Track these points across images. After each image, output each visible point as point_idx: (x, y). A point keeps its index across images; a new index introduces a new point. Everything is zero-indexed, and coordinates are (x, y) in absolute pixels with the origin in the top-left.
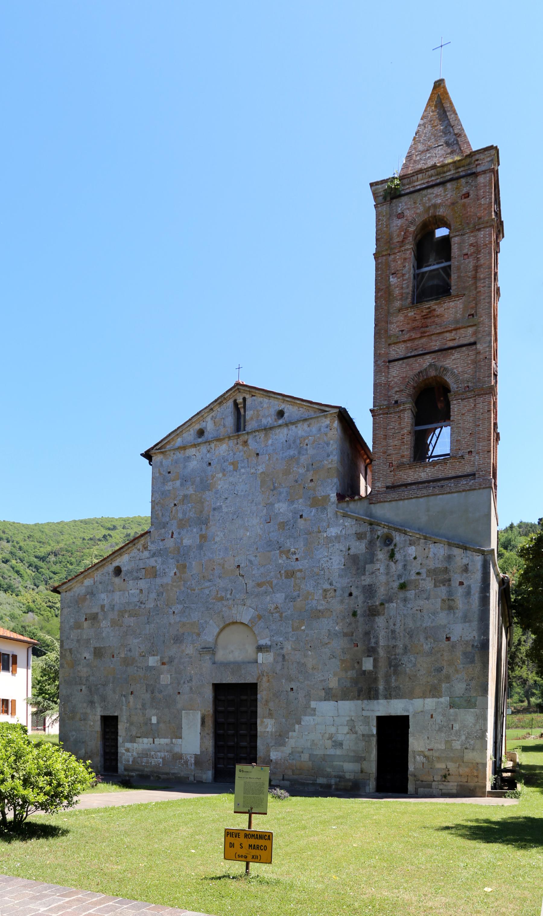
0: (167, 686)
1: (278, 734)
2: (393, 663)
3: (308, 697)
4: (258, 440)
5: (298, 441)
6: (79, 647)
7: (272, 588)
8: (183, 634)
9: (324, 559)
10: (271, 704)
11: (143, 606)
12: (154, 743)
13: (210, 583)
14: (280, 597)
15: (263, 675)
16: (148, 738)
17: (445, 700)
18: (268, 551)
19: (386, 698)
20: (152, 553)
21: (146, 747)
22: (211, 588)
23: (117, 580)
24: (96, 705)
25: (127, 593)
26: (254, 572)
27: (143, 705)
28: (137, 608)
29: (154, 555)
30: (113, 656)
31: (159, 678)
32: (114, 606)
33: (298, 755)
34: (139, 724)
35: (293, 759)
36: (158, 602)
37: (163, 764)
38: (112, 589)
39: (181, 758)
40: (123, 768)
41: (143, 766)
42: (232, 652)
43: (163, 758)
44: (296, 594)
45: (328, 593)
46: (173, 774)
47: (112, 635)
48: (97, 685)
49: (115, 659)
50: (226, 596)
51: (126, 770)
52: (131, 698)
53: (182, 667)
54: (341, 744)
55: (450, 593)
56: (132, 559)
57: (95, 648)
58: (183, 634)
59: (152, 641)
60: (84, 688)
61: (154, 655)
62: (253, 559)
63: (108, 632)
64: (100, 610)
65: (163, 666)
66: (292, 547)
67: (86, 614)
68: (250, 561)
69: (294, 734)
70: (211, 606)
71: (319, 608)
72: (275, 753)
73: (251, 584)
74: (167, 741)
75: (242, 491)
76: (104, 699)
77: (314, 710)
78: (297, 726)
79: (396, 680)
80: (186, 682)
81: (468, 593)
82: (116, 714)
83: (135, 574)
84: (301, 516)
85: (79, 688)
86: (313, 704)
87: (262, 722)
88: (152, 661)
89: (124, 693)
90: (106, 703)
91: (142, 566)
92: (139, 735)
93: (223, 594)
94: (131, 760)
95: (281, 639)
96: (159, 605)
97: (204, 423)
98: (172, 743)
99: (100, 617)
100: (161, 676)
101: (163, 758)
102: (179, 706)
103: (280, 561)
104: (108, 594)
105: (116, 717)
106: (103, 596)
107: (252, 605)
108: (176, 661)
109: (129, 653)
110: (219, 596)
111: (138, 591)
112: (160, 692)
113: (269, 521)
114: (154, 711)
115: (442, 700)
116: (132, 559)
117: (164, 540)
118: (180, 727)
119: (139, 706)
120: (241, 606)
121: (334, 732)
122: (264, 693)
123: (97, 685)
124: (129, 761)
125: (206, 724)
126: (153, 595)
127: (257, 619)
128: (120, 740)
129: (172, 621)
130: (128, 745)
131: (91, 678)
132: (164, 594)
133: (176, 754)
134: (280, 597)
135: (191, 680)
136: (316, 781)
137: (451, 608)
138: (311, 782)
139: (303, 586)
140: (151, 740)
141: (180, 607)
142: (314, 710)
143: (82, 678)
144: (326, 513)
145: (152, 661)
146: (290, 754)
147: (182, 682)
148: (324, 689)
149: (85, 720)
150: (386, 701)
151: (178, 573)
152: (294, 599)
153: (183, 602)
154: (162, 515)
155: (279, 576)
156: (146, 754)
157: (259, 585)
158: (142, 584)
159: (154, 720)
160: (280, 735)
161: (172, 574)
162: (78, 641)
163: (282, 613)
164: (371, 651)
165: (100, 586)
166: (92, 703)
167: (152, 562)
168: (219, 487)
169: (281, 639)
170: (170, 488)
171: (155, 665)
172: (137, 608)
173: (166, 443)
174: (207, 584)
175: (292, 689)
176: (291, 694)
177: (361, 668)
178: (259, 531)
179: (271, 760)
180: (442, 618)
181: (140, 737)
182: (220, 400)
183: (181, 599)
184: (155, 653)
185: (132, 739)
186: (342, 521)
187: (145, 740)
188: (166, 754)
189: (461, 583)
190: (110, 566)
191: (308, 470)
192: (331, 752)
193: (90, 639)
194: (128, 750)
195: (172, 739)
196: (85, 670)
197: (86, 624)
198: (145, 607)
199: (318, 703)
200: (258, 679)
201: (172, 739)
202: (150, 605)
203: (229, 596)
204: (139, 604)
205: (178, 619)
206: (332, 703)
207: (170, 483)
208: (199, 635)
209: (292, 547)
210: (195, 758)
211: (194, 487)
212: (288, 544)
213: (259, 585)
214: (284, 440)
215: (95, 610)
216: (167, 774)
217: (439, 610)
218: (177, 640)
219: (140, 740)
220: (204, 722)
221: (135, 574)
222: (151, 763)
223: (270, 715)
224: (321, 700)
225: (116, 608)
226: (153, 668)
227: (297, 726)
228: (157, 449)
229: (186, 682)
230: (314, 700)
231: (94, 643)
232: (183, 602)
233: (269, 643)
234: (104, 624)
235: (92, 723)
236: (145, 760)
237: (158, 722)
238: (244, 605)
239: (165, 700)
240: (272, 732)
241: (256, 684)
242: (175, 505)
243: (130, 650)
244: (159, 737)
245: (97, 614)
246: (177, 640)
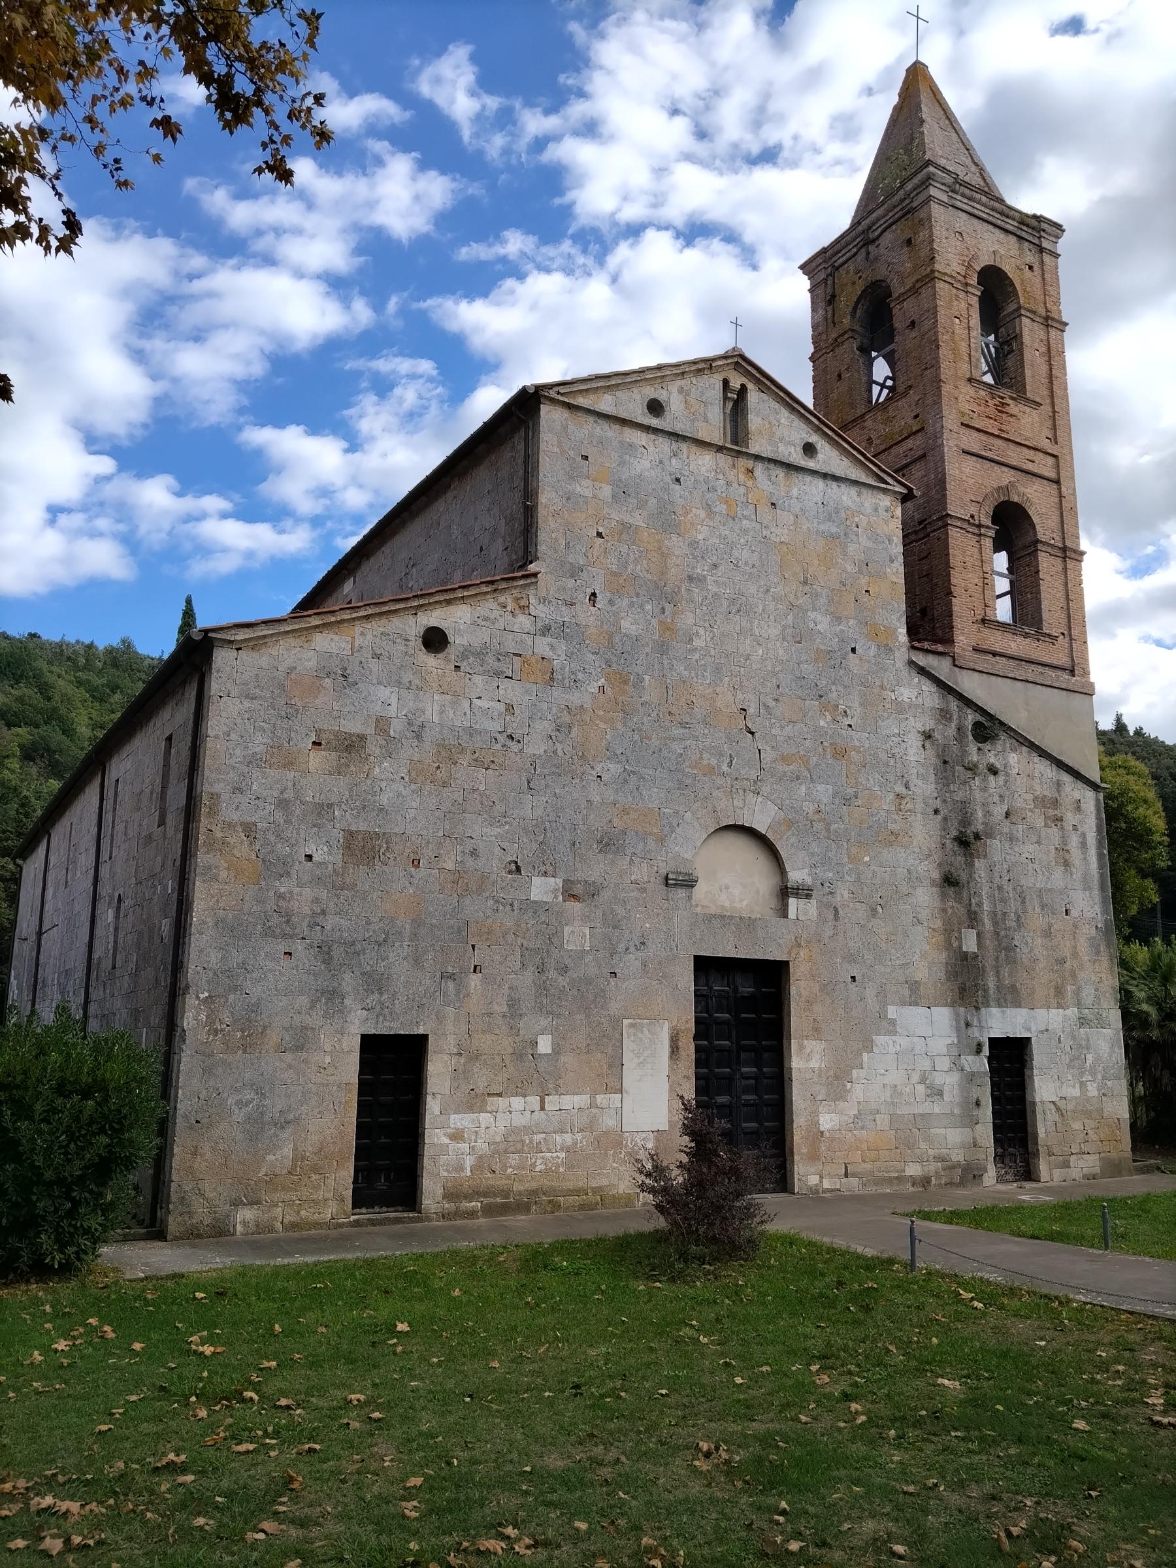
0: (582, 954)
1: (832, 1073)
2: (1004, 944)
3: (882, 996)
4: (773, 478)
5: (843, 515)
6: (288, 822)
7: (808, 770)
8: (624, 832)
9: (893, 739)
10: (818, 1009)
11: (515, 747)
12: (542, 1108)
13: (683, 731)
14: (823, 791)
15: (799, 946)
16: (524, 1096)
17: (1072, 1012)
18: (799, 697)
19: (1000, 1006)
20: (540, 624)
21: (519, 1120)
22: (688, 743)
23: (431, 661)
24: (347, 1002)
25: (466, 704)
26: (773, 731)
27: (513, 1003)
28: (498, 747)
29: (546, 630)
30: (416, 863)
31: (558, 933)
32: (422, 726)
33: (871, 1117)
34: (498, 1059)
35: (862, 1128)
36: (559, 747)
37: (570, 1167)
38: (417, 682)
39: (619, 1144)
40: (440, 1192)
41: (508, 1177)
42: (727, 888)
43: (568, 1150)
44: (851, 791)
45: (904, 802)
46: (596, 1190)
47: (414, 805)
48: (353, 944)
49: (422, 872)
50: (719, 767)
51: (449, 1196)
52: (475, 980)
53: (619, 910)
54: (940, 1093)
55: (1064, 840)
56: (480, 621)
57: (350, 834)
58: (624, 832)
59: (540, 839)
60: (299, 948)
61: (546, 874)
62: (772, 704)
63: (399, 795)
64: (370, 731)
65: (569, 905)
66: (841, 702)
67: (318, 732)
68: (767, 707)
69: (862, 1073)
70: (687, 782)
71: (891, 826)
72: (827, 1117)
73: (768, 755)
74: (581, 1100)
75: (747, 562)
76: (376, 983)
77: (893, 1022)
78: (865, 1056)
79: (1011, 974)
80: (632, 949)
81: (1084, 844)
82: (421, 1032)
83: (491, 661)
84: (853, 650)
85: (283, 947)
86: (892, 1011)
87: (801, 1047)
88: (541, 888)
89: (450, 969)
90: (386, 996)
91: (511, 647)
92: (496, 1089)
93: (714, 762)
94: (469, 1162)
95: (831, 875)
96: (560, 753)
97: (664, 392)
98: (593, 1105)
99: (373, 747)
100: (566, 929)
101: (568, 1150)
102: (614, 1008)
103: (822, 723)
104: (404, 692)
105: (424, 1038)
106: (384, 693)
107: (773, 797)
108: (606, 895)
109: (470, 862)
110: (705, 762)
111: (501, 707)
112: (564, 970)
113: (798, 639)
114: (544, 1022)
115: (1069, 1012)
116: (480, 621)
117: (573, 604)
118: (617, 1064)
119: (501, 1007)
120: (751, 794)
121: (928, 1069)
122: (803, 983)
123: (353, 944)
124: (462, 1169)
125: (682, 1053)
126: (543, 726)
127: (783, 828)
128: (432, 1106)
129: (596, 798)
130: (459, 1120)
131: (330, 922)
132: (575, 730)
133: (607, 1133)
134: (823, 791)
135: (643, 943)
136: (904, 1171)
137: (1066, 864)
138: (896, 1175)
139: (862, 780)
140: (534, 1101)
141: (615, 768)
142: (893, 1022)
143: (295, 919)
144: (892, 657)
145: (541, 888)
146: (856, 1117)
147: (622, 946)
148: (906, 982)
149: (299, 1048)
150: (1000, 1010)
151: (608, 689)
152: (847, 801)
153: (623, 758)
154: (567, 545)
155: (820, 749)
156: (514, 1139)
157: (785, 759)
158: (512, 691)
159: (545, 1045)
160: (837, 1077)
161: (593, 688)
162: (283, 804)
163: (829, 824)
164: (973, 919)
165: (374, 665)
166: (332, 996)
167: (542, 646)
168: (700, 537)
169: (831, 875)
170: (588, 493)
171: (548, 898)
172: (498, 747)
173: (581, 391)
174: (678, 731)
175: (853, 978)
176: (852, 986)
177: (960, 947)
178: (781, 652)
179: (822, 1133)
180: (1058, 878)
181: (500, 1095)
182: (700, 366)
183: (619, 752)
184: (550, 869)
185: (475, 1102)
186: (916, 680)
187: (517, 1102)
188: (579, 1136)
189: (1075, 828)
190: (411, 620)
191: (860, 572)
192: (926, 1108)
193: (330, 806)
194: (457, 1136)
195: (594, 1094)
196: (308, 893)
197: (316, 760)
198: (521, 750)
199: (899, 1009)
200: (789, 953)
201: (594, 1094)
202: (536, 747)
203: (725, 768)
204: (502, 739)
205: (610, 795)
206: (922, 1010)
207: (586, 482)
208: (661, 840)
209: (841, 702)
210: (657, 1140)
211: (645, 513)
212: (834, 695)
213: (785, 759)
214: (819, 499)
215: (353, 726)
216: (577, 1192)
217: (1053, 863)
218: (607, 844)
219: (501, 1102)
220: (677, 1048)
221: (491, 661)
222: (534, 1165)
223: (817, 1032)
224: (903, 1004)
225: (428, 734)
226: (538, 907)
227: (865, 1056)
228: (558, 393)
229: (632, 949)
230: (893, 1004)
231: (344, 818)
232: (623, 758)
233: (809, 880)
234: (383, 769)
235: (328, 1059)
236: (514, 1159)
237: (557, 1051)
238: (758, 793)
239: (575, 992)
240: (820, 1068)
241: (787, 962)
242: (599, 535)
243: (474, 853)
244: (557, 1091)
245: (362, 737)
246: (607, 844)
